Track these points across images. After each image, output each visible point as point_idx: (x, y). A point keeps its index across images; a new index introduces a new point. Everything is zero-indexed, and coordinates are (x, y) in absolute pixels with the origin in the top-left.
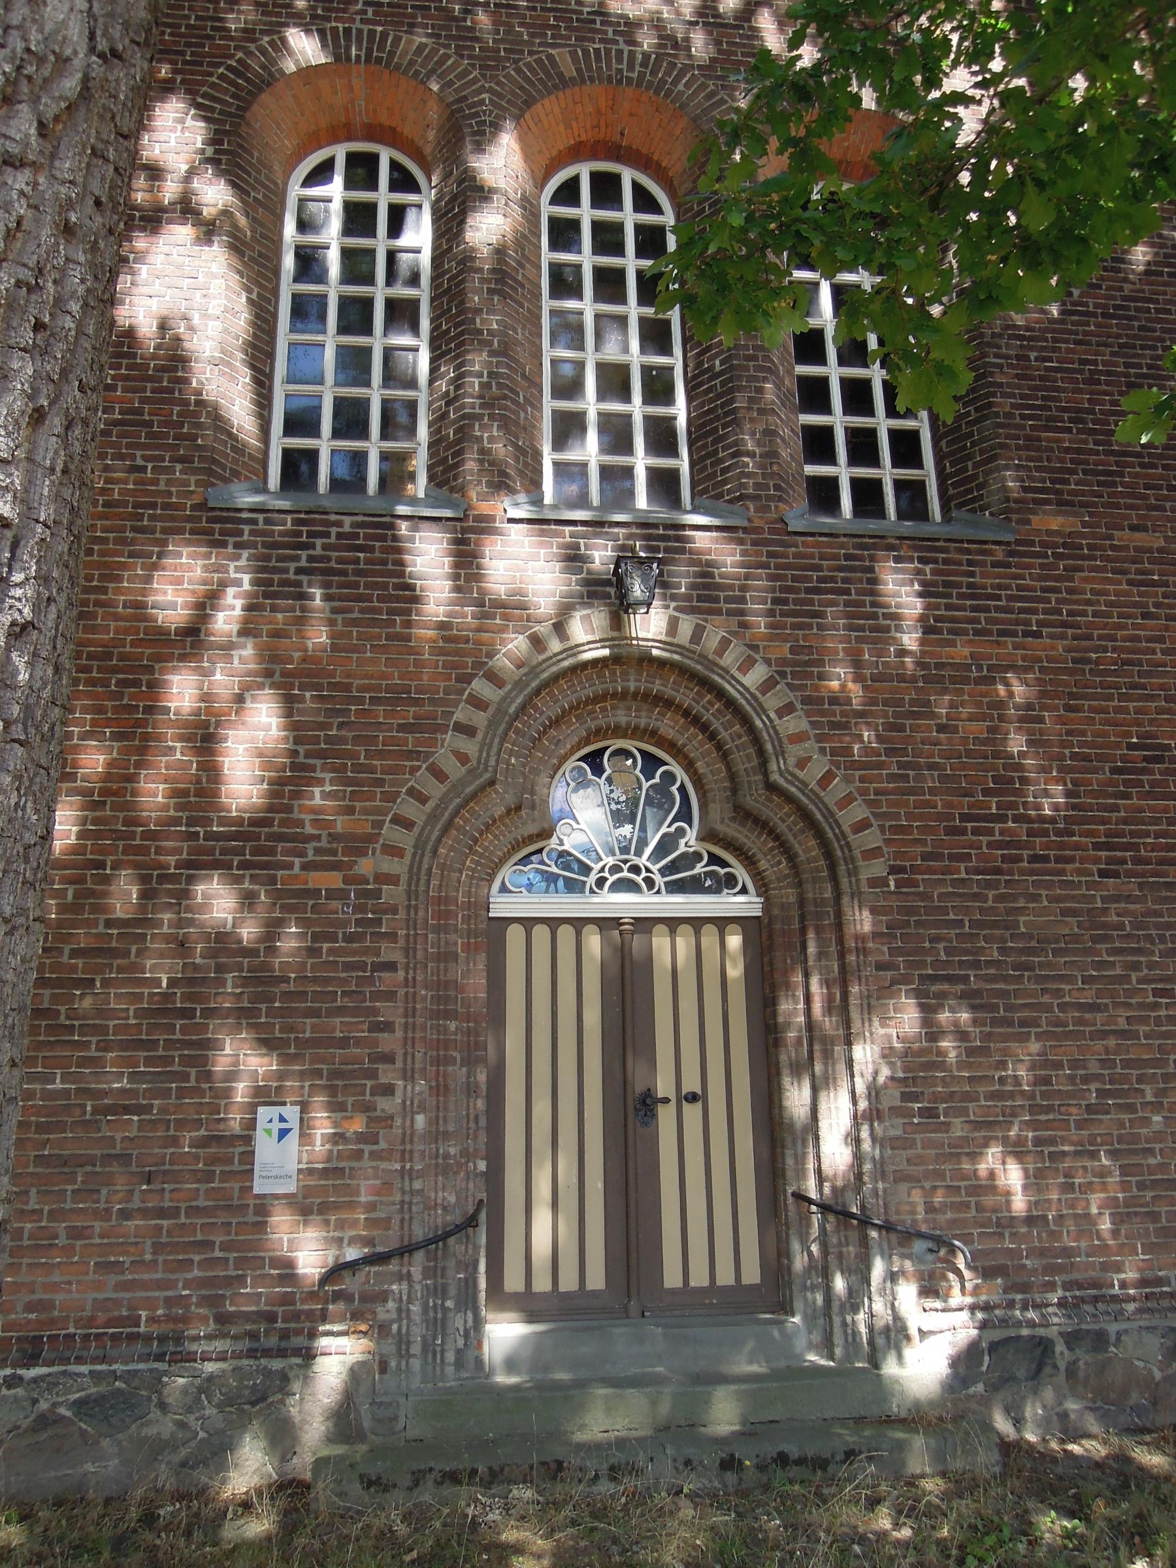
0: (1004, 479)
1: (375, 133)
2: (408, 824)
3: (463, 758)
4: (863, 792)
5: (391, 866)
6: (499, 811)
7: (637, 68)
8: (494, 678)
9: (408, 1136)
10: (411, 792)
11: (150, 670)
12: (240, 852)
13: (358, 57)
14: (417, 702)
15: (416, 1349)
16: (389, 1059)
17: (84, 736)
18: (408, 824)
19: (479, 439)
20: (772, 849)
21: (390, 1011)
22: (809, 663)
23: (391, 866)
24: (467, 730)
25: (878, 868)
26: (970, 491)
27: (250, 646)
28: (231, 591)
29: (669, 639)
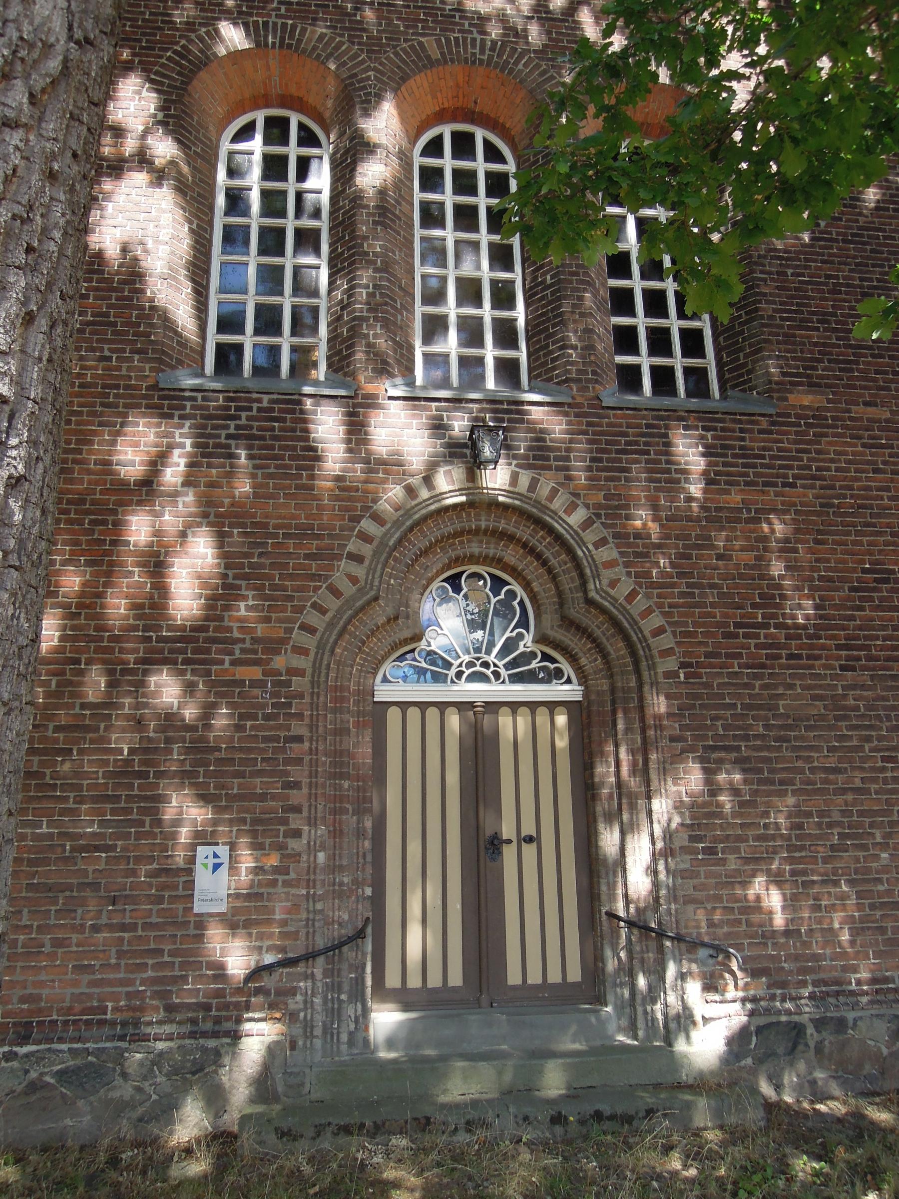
0: (767, 366)
1: (286, 102)
2: (312, 630)
3: (354, 580)
4: (660, 606)
5: (299, 662)
6: (382, 620)
7: (487, 52)
9: (312, 869)
10: (314, 606)
11: (114, 512)
12: (183, 651)
13: (274, 44)
14: (319, 537)
15: (318, 1031)
16: (297, 809)
17: (64, 563)
18: (312, 630)
19: (367, 336)
20: (590, 649)
21: (298, 773)
22: (619, 507)
23: (299, 662)
24: (357, 558)
25: (671, 664)
26: (742, 375)
27: (191, 494)
28: (176, 452)
29: (511, 489)
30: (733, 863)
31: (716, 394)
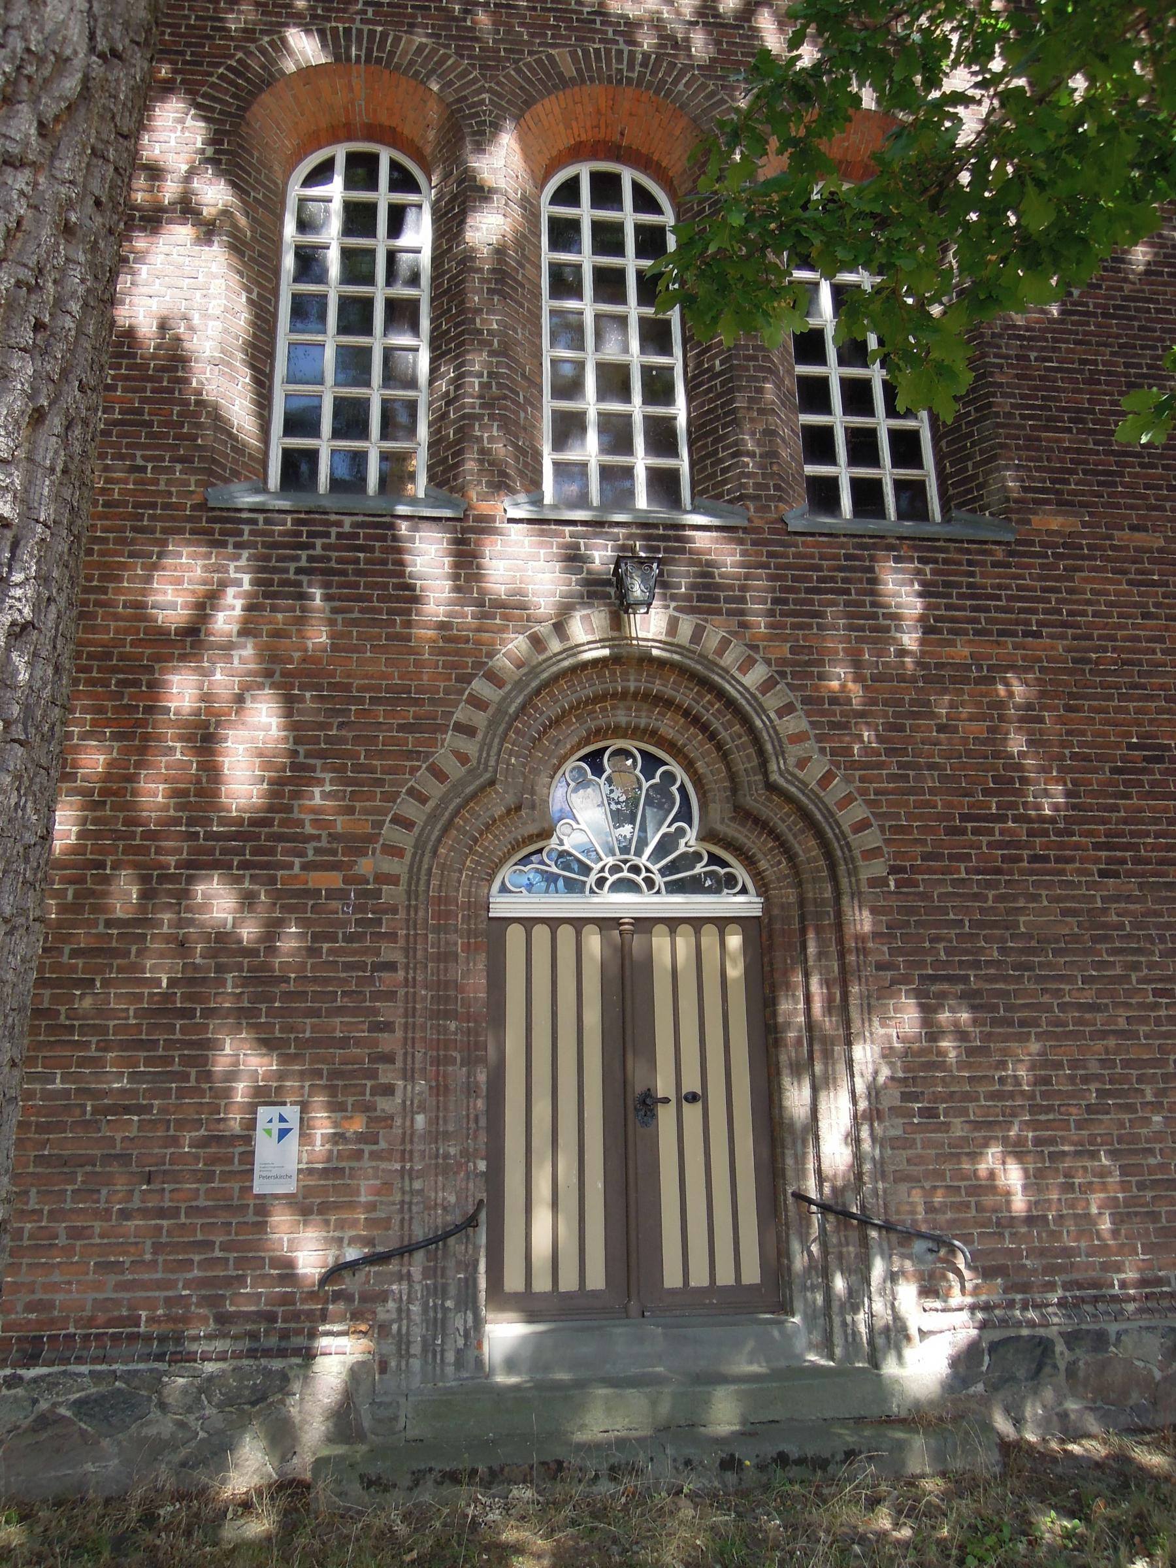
0: (1004, 479)
1: (375, 133)
2: (408, 824)
3: (463, 758)
4: (863, 792)
5: (391, 866)
6: (499, 811)
7: (637, 68)
8: (494, 678)
9: (408, 1136)
10: (411, 792)
11: (150, 670)
12: (240, 852)
13: (358, 57)
14: (417, 702)
15: (416, 1349)
16: (389, 1059)
17: (84, 736)
18: (408, 824)
19: (479, 439)
20: (772, 849)
21: (390, 1011)
22: (809, 663)
23: (391, 866)
24: (467, 730)
25: (878, 868)
26: (970, 491)
27: (250, 646)
28: (231, 591)
29: (669, 639)
30: (959, 1129)
31: (937, 515)
